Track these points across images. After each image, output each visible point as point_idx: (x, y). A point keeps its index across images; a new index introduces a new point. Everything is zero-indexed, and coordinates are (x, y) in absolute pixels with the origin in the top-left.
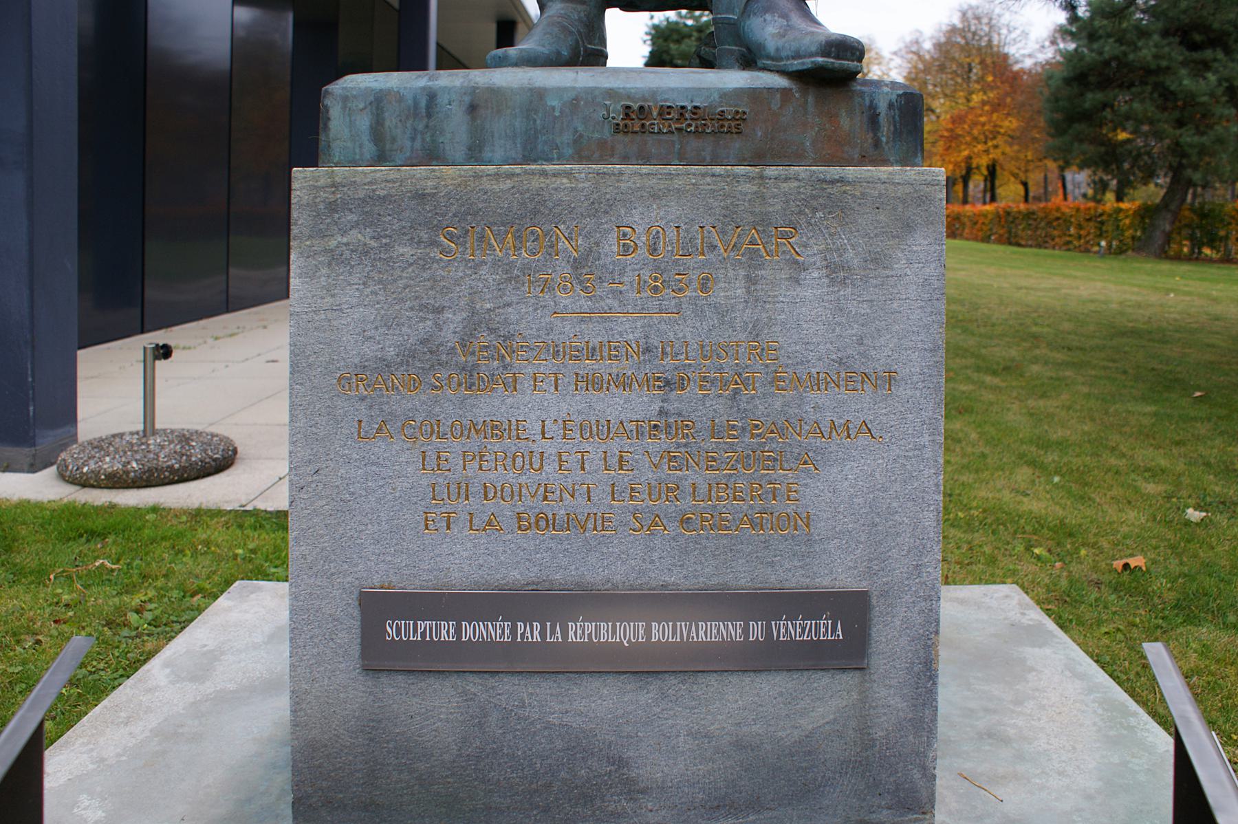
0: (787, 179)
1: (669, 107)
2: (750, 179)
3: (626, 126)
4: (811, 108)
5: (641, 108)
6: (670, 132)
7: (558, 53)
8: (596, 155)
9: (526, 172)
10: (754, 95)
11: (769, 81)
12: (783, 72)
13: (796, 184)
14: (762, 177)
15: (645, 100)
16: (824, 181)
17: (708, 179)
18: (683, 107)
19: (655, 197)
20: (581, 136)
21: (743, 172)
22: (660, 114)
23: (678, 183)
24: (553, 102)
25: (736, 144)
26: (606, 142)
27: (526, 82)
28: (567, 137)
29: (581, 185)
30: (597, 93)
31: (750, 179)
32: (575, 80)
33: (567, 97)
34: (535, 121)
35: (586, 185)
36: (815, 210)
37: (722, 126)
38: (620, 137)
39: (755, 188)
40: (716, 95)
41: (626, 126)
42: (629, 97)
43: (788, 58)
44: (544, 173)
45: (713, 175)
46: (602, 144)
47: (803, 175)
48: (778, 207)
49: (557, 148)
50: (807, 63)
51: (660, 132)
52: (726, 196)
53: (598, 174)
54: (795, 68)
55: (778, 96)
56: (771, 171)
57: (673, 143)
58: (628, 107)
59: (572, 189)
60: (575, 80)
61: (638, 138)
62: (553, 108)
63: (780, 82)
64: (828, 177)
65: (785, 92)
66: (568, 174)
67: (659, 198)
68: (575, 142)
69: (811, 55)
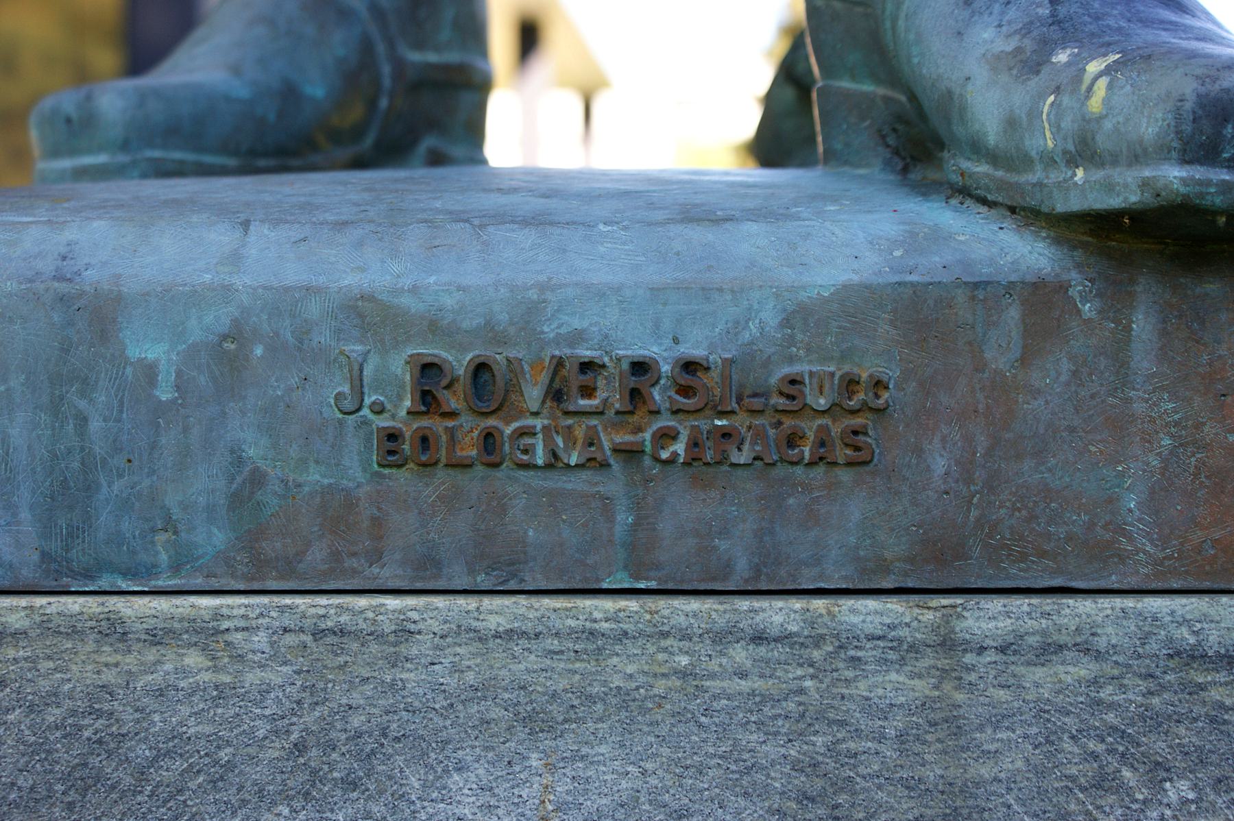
0: (1049, 650)
1: (587, 366)
2: (902, 651)
3: (424, 441)
4: (1143, 360)
5: (481, 369)
6: (594, 464)
7: (289, 94)
8: (317, 554)
9: (47, 627)
10: (925, 313)
11: (979, 252)
12: (1028, 214)
13: (1084, 669)
14: (948, 644)
15: (501, 339)
16: (1194, 657)
17: (740, 654)
18: (640, 367)
19: (535, 722)
20: (257, 479)
21: (873, 625)
22: (556, 395)
23: (624, 667)
24: (148, 347)
25: (853, 517)
26: (350, 503)
27: (47, 266)
28: (205, 483)
29: (252, 678)
30: (314, 309)
31: (902, 651)
32: (235, 259)
33: (205, 324)
34: (82, 420)
35: (276, 675)
36: (1158, 773)
37: (793, 440)
38: (403, 478)
39: (922, 687)
40: (770, 317)
41: (424, 441)
42: (434, 327)
43: (1049, 161)
44: (114, 632)
45: (759, 638)
46: (337, 512)
47: (1110, 635)
48: (1013, 762)
49: (170, 525)
50: (1124, 189)
51: (554, 462)
52: (806, 721)
53: (318, 634)
54: (1074, 204)
55: (1013, 313)
56: (988, 619)
57: (607, 504)
58: (428, 369)
59: (221, 693)
60: (235, 259)
61: (474, 483)
62: (150, 372)
63: (1026, 253)
64: (1214, 640)
65: (1041, 297)
66: (207, 635)
67: (550, 727)
68: (237, 500)
69: (1138, 156)
